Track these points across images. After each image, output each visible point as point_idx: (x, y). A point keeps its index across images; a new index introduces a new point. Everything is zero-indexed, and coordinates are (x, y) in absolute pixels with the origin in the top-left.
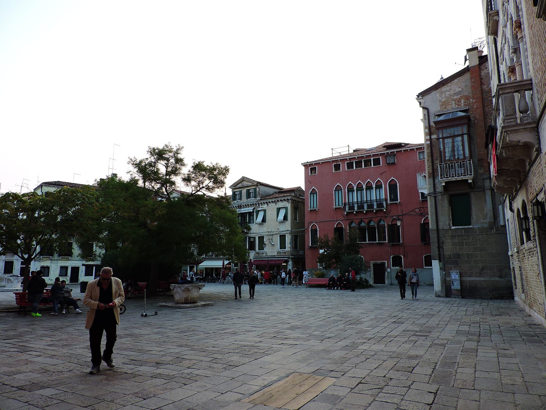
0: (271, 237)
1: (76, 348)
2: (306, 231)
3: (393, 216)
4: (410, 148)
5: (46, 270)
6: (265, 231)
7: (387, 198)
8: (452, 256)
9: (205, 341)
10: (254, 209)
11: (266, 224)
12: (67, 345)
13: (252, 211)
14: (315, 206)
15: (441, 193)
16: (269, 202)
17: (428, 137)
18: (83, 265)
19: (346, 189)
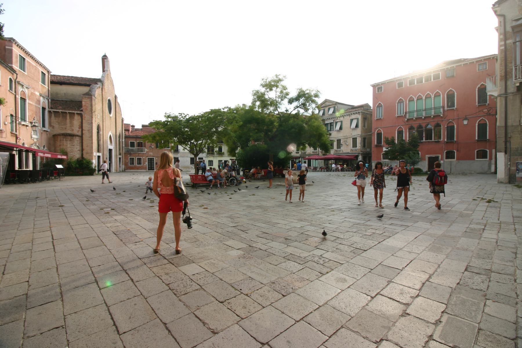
0: (346, 140)
1: (222, 217)
2: (373, 134)
3: (449, 120)
4: (470, 62)
5: (211, 162)
6: (342, 135)
7: (445, 105)
8: (519, 149)
9: (319, 216)
10: (334, 121)
11: (342, 131)
12: (217, 213)
13: (333, 122)
14: (381, 116)
15: (513, 93)
16: (345, 115)
17: (503, 43)
18: (230, 159)
19: (408, 101)
